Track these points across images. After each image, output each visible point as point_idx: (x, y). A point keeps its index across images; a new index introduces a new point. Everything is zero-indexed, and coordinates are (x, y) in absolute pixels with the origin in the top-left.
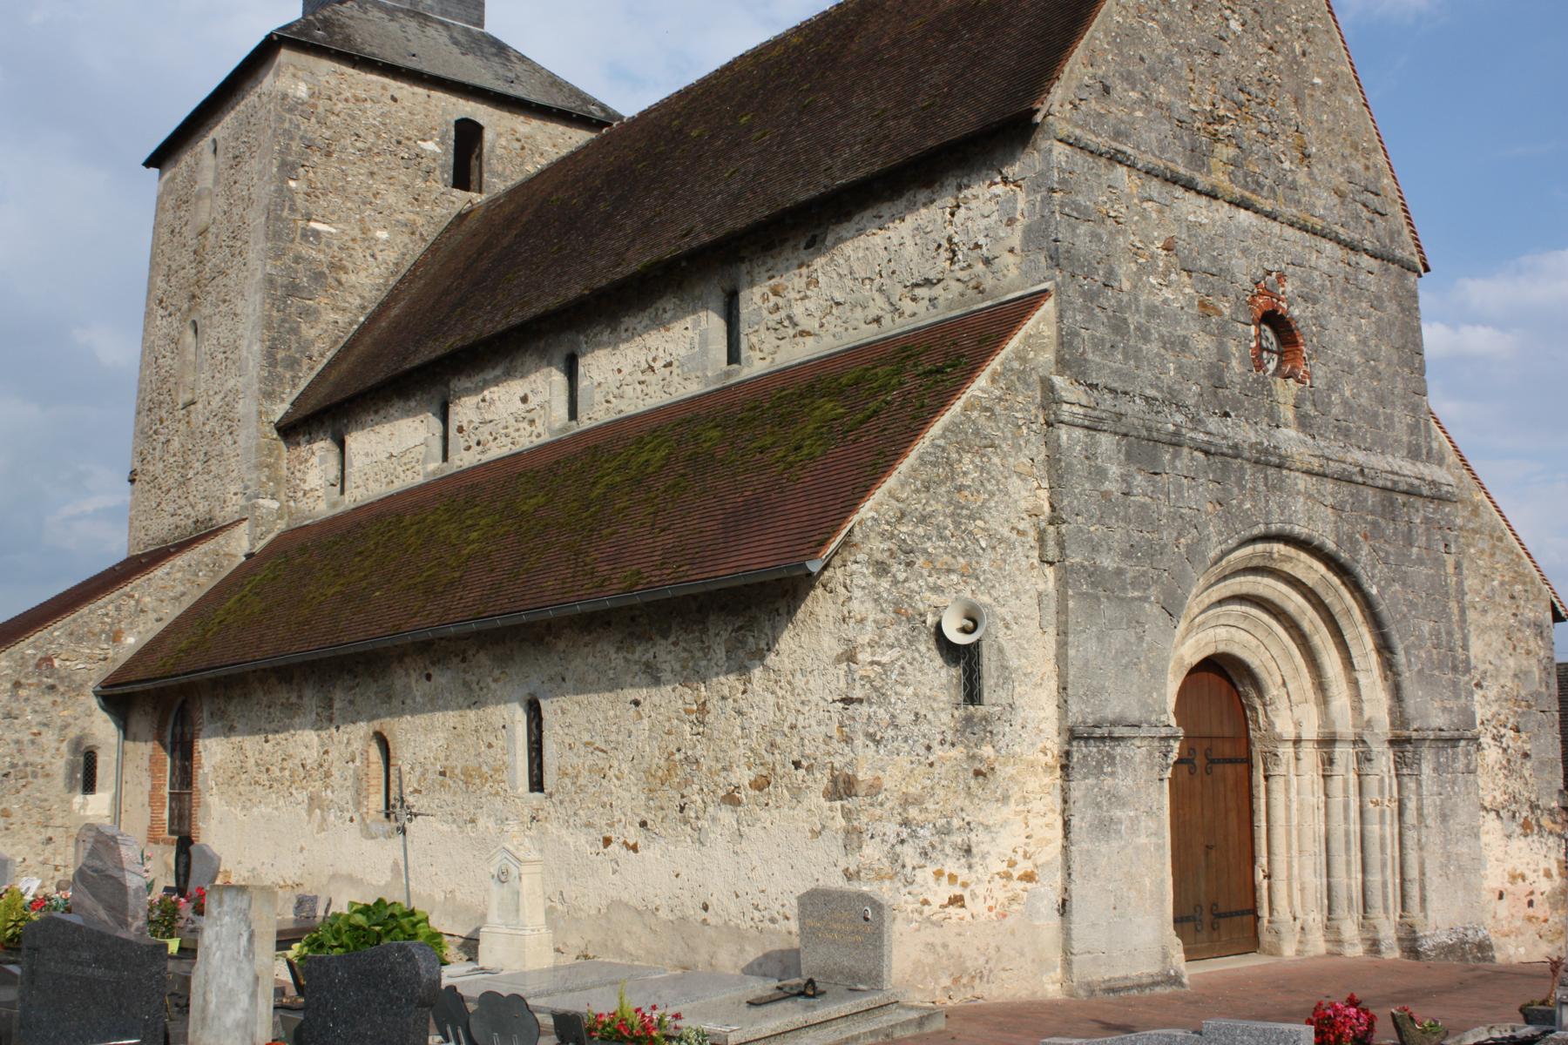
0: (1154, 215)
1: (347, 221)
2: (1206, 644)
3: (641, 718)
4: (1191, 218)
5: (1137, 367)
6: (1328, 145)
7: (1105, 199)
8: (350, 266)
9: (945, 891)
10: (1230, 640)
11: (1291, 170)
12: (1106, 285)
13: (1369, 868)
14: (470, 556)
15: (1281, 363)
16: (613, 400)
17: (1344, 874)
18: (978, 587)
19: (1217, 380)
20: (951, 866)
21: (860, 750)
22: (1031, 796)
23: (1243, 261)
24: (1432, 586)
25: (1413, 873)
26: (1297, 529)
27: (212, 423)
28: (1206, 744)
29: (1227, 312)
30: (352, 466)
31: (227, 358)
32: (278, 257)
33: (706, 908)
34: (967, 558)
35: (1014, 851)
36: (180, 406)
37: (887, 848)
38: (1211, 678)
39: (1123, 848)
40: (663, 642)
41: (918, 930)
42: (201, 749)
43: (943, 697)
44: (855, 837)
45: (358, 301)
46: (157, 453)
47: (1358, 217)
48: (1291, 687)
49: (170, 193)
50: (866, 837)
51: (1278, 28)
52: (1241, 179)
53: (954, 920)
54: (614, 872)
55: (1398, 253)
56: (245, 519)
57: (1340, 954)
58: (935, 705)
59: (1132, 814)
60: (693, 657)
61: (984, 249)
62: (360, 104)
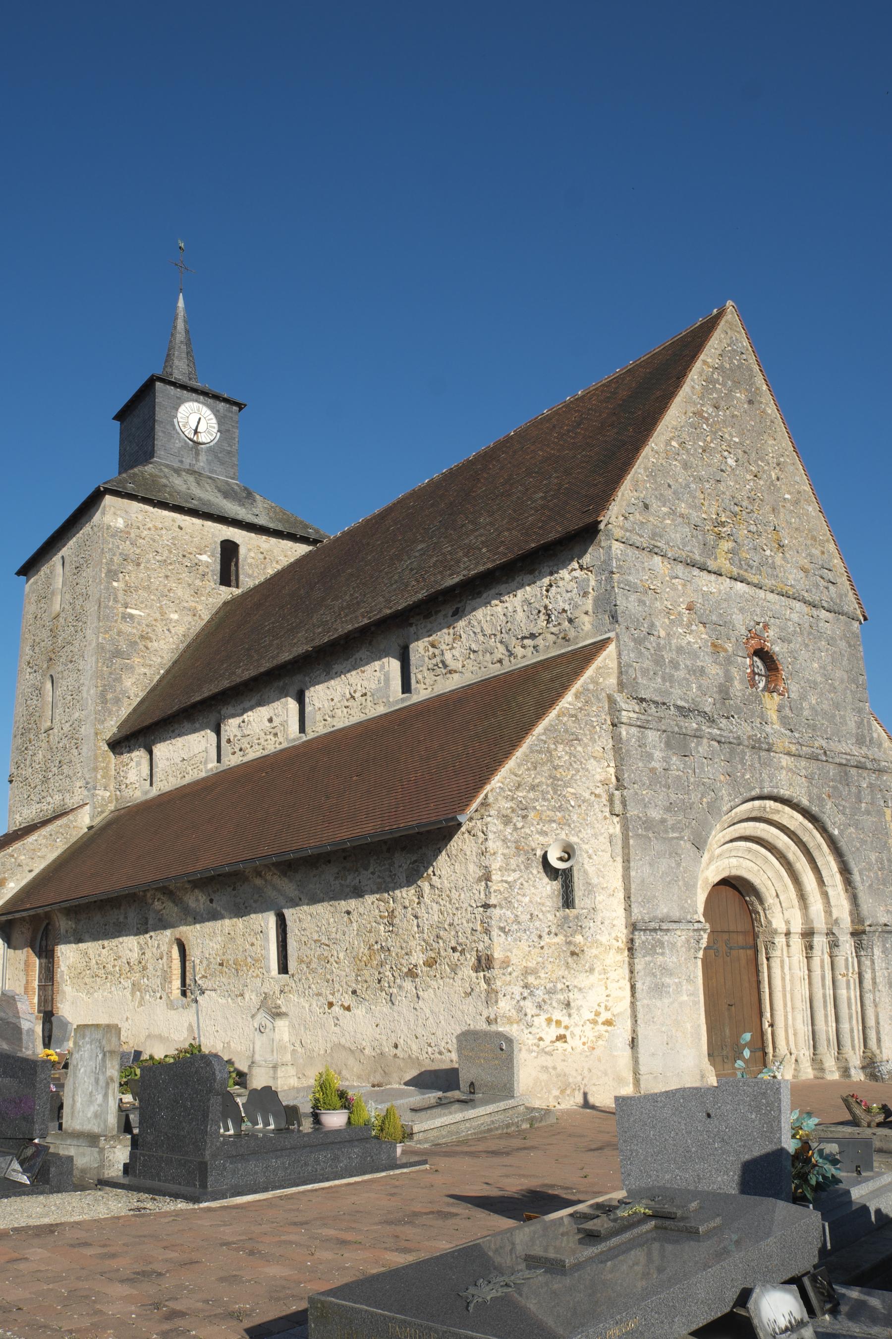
0: (680, 587)
1: (151, 607)
2: (723, 869)
3: (352, 923)
4: (705, 589)
5: (671, 687)
6: (796, 538)
7: (647, 577)
8: (154, 638)
9: (553, 1032)
10: (737, 867)
11: (771, 556)
12: (649, 634)
13: (841, 1020)
14: (319, 627)
15: (768, 682)
16: (329, 719)
17: (823, 1023)
18: (570, 832)
19: (724, 693)
20: (557, 1015)
21: (495, 938)
22: (609, 969)
23: (740, 617)
24: (876, 829)
25: (871, 1022)
26: (782, 792)
27: (65, 741)
28: (726, 936)
29: (730, 650)
30: (157, 767)
31: (73, 699)
32: (106, 632)
33: (396, 1046)
34: (562, 813)
35: (599, 1005)
36: (43, 731)
37: (514, 1002)
38: (727, 891)
39: (672, 1003)
40: (364, 872)
41: (536, 1057)
42: (59, 954)
43: (549, 903)
44: (493, 995)
45: (159, 660)
46: (28, 763)
47: (817, 586)
48: (782, 898)
49: (33, 592)
50: (500, 995)
51: (760, 463)
52: (737, 562)
53: (560, 1049)
54: (336, 1025)
55: (846, 609)
56: (87, 804)
57: (823, 1078)
58: (544, 909)
59: (676, 980)
60: (384, 882)
61: (569, 612)
62: (160, 532)
